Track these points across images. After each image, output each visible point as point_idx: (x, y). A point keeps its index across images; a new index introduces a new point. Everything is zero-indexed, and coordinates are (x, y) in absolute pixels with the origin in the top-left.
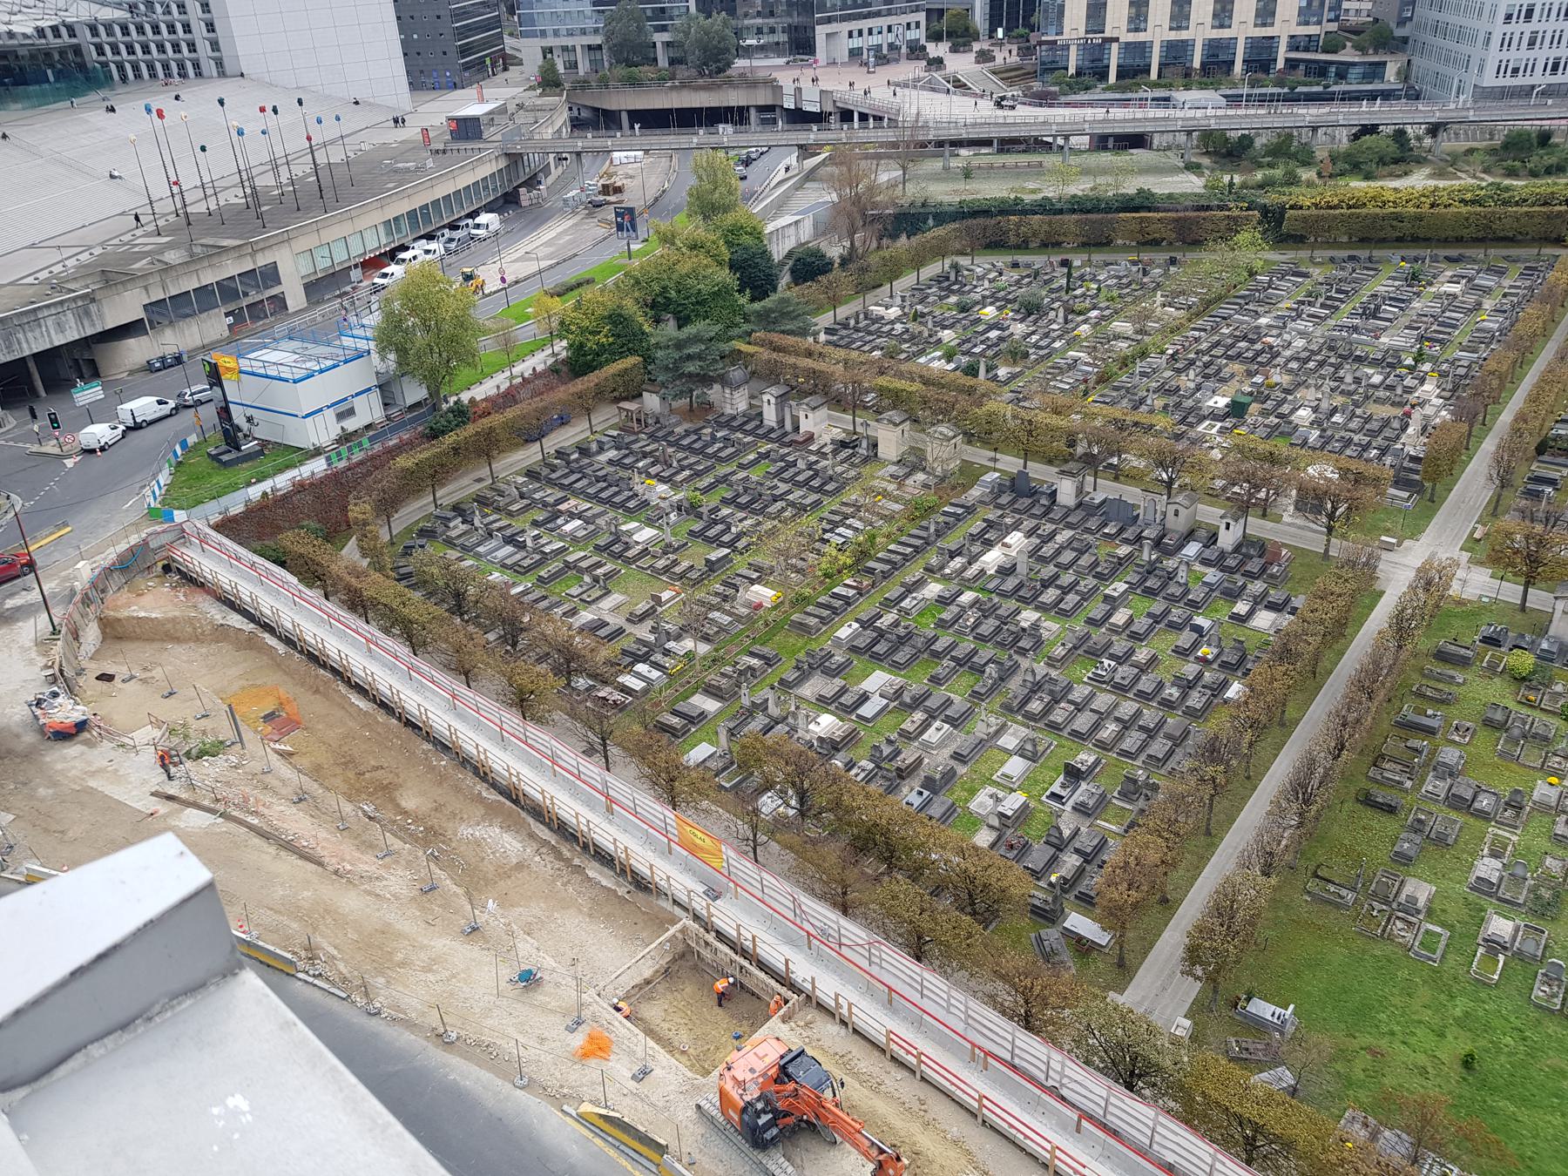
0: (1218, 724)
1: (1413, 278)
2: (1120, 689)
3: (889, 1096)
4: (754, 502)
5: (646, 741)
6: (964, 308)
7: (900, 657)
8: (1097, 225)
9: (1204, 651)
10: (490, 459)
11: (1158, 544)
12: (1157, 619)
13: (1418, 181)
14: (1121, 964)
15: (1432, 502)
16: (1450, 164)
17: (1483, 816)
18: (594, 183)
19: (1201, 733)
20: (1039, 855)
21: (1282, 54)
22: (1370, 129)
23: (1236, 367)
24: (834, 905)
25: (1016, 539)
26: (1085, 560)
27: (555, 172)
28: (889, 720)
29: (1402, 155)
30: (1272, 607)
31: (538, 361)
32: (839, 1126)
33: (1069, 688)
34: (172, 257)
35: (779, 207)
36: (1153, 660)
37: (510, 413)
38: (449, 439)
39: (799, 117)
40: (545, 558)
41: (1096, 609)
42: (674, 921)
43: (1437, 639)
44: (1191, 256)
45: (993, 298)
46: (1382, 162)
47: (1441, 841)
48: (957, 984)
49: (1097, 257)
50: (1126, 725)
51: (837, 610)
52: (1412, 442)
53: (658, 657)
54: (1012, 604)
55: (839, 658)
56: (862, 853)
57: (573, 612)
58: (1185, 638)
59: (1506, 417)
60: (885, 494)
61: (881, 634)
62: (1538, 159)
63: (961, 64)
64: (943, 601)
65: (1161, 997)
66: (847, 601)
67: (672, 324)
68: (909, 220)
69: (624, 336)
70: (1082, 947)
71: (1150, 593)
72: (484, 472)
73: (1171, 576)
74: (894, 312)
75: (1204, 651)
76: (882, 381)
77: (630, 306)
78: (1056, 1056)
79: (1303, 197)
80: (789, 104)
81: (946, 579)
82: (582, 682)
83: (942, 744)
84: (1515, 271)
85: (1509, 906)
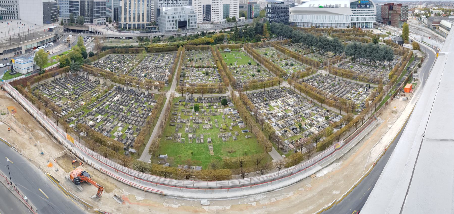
0: (149, 119)
1: (163, 56)
2: (134, 116)
3: (101, 178)
4: (83, 89)
5: (64, 123)
6: (111, 62)
7: (103, 113)
8: (127, 50)
9: (145, 109)
10: (47, 78)
11: (138, 95)
12: (138, 106)
13: (162, 43)
14: (138, 155)
15: (170, 85)
16: (164, 41)
17: (185, 123)
18: (66, 39)
19: (146, 121)
20: (124, 141)
21: (145, 26)
22: (155, 37)
23: (144, 70)
24: (92, 150)
25: (119, 95)
26: (128, 98)
27: (61, 37)
28: (101, 122)
29: (159, 40)
30: (153, 102)
31: (55, 65)
32: (91, 182)
33: (127, 117)
34: (8, 44)
35: (88, 45)
36: (139, 112)
37: (51, 72)
38: (42, 75)
39: (91, 32)
40: (53, 94)
41: (130, 105)
42: (65, 149)
43: (175, 103)
44: (138, 54)
45: (114, 60)
46: (157, 41)
47: (181, 128)
48: (113, 161)
49: (127, 55)
50: (136, 121)
51: (94, 106)
52: (167, 78)
53: (67, 111)
54: (119, 105)
55: (94, 113)
56: (96, 142)
57: (55, 102)
58: (143, 108)
59: (176, 73)
60: (101, 89)
61: (100, 110)
62: (173, 40)
63: (110, 26)
64: (109, 105)
65: (145, 158)
66: (95, 105)
67: (74, 62)
68: (104, 49)
69: (68, 63)
70: (132, 153)
71: (137, 102)
72: (46, 80)
73: (140, 99)
74: (102, 62)
75: (145, 109)
76: (101, 72)
77: (69, 58)
78: (130, 170)
79: (149, 46)
80: (90, 30)
81: (109, 102)
82: (55, 113)
83: (109, 126)
84: (173, 54)
85: (191, 133)
